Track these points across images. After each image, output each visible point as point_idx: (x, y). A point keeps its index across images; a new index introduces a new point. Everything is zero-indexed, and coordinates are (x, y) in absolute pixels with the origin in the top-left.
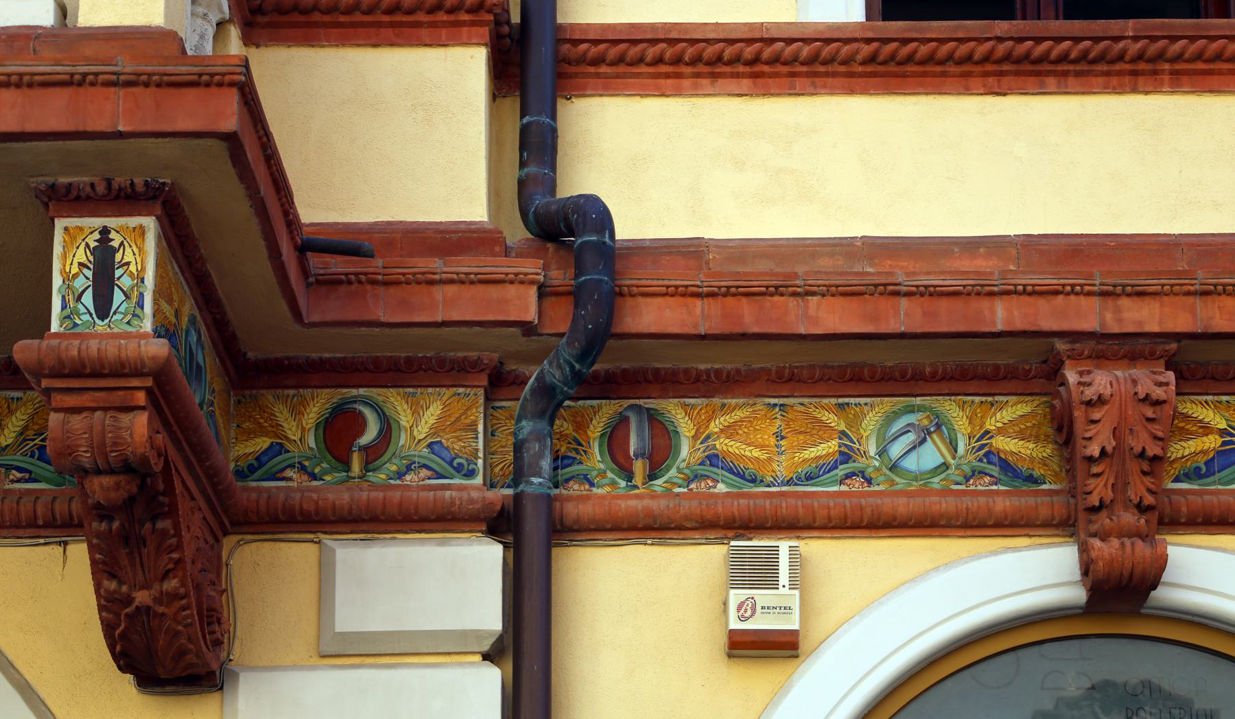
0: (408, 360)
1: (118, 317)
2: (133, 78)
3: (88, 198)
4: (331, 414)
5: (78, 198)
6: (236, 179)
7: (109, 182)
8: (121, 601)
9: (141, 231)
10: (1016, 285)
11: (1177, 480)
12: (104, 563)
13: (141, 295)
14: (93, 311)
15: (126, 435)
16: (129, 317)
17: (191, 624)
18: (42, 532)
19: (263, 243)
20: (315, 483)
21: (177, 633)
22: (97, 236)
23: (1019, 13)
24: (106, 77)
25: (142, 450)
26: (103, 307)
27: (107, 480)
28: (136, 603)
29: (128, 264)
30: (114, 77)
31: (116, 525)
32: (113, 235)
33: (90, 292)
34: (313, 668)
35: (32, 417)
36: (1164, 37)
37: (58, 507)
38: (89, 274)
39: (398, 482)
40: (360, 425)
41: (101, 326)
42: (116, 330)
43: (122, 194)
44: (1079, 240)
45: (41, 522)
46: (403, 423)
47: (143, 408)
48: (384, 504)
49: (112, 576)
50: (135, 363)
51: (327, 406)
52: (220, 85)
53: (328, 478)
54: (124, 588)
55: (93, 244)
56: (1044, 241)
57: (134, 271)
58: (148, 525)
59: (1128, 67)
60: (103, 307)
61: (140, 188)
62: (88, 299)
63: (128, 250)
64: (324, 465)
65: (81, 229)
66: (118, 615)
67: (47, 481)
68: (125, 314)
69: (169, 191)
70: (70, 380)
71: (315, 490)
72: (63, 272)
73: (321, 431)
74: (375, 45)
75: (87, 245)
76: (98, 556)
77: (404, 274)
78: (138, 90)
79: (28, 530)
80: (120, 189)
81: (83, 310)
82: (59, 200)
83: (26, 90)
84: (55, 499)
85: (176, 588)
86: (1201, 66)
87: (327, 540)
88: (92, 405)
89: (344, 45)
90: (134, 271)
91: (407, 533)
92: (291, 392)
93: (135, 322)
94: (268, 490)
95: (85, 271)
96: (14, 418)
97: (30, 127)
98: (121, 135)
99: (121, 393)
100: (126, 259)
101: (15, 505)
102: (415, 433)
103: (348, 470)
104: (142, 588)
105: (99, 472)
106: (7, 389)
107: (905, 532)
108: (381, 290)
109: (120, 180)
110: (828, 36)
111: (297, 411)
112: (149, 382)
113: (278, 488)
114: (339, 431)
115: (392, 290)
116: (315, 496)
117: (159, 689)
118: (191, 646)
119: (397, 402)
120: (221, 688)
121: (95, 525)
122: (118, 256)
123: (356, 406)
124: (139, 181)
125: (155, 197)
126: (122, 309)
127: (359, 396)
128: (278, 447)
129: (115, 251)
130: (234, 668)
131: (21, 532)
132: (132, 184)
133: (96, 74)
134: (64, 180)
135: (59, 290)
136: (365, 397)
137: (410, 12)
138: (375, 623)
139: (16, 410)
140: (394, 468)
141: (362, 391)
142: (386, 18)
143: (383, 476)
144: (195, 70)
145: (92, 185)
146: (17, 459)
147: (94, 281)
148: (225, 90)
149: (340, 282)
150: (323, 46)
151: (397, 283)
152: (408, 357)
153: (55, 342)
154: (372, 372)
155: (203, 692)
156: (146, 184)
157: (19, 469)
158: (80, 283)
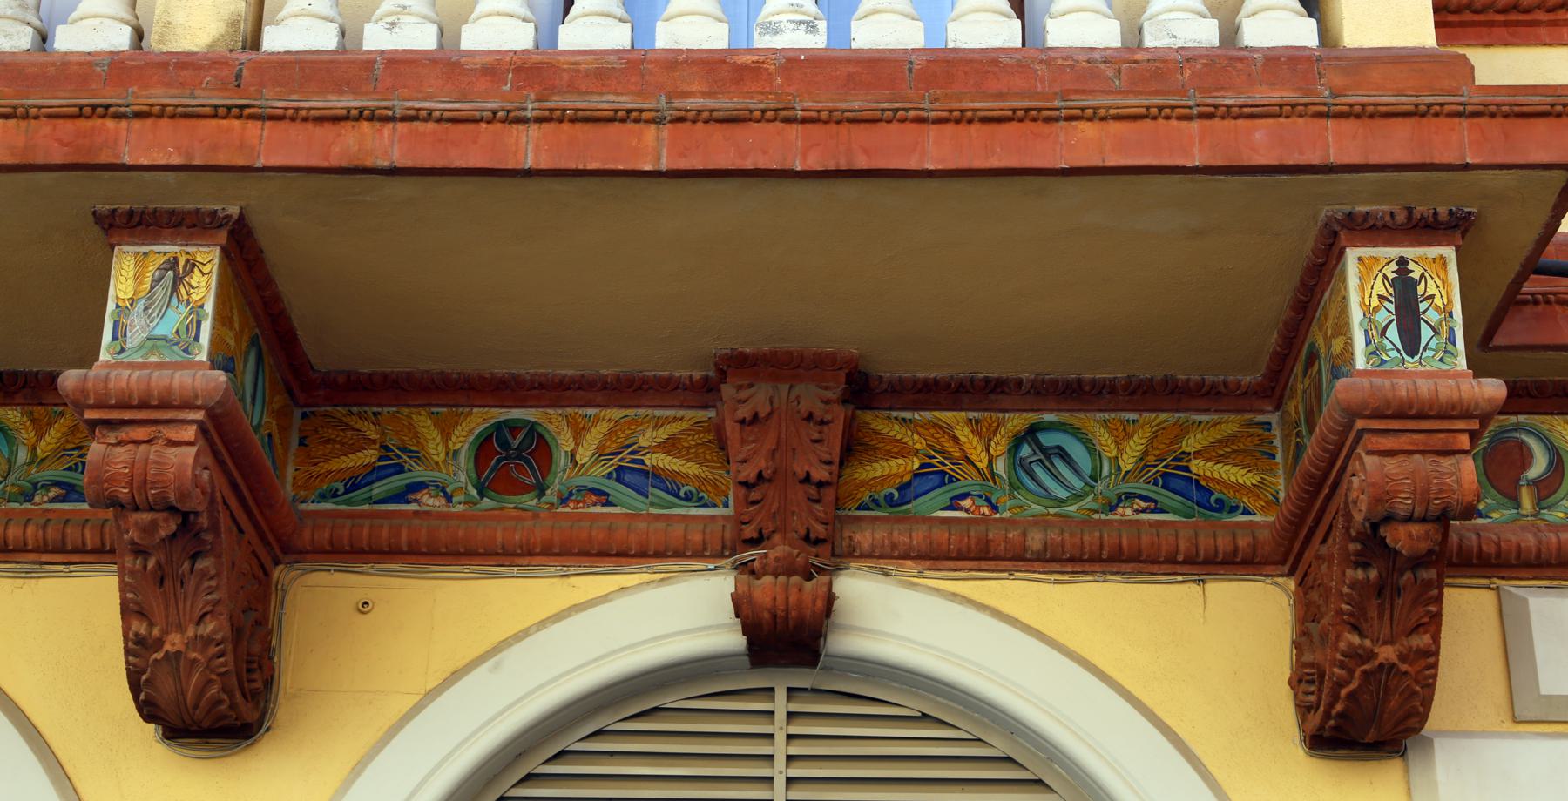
1: (1428, 353)
3: (1385, 226)
6: (1550, 207)
7: (1410, 210)
9: (1443, 261)
12: (1351, 614)
13: (1451, 330)
16: (1441, 354)
18: (1179, 569)
19: (1518, 268)
21: (1415, 693)
24: (1454, 107)
26: (1411, 344)
27: (1416, 529)
28: (1381, 659)
29: (1432, 297)
30: (1461, 108)
31: (1373, 574)
32: (1411, 266)
35: (1151, 441)
38: (1391, 307)
40: (1526, 459)
41: (1411, 363)
42: (1428, 368)
45: (1180, 558)
47: (1465, 452)
49: (1355, 628)
53: (1495, 515)
54: (1368, 643)
55: (1391, 276)
58: (1408, 575)
60: (1411, 344)
62: (1393, 333)
63: (1430, 282)
64: (1489, 501)
65: (1376, 259)
66: (1351, 672)
67: (1175, 512)
72: (1362, 304)
78: (1483, 121)
80: (1422, 218)
81: (1389, 346)
83: (1367, 121)
93: (1448, 359)
97: (1374, 159)
98: (1466, 167)
99: (1442, 436)
103: (1518, 506)
104: (1385, 643)
105: (1409, 519)
109: (1421, 210)
112: (199, 415)
116: (1494, 538)
117: (1330, 753)
121: (1349, 572)
122: (1420, 289)
123: (1524, 437)
124: (1443, 211)
125: (1456, 226)
127: (1518, 424)
129: (1415, 283)
131: (1155, 568)
132: (1435, 214)
133: (1441, 105)
135: (1361, 324)
137: (1527, 11)
139: (1134, 432)
141: (1522, 418)
142: (1501, 18)
144: (1549, 99)
146: (1140, 487)
147: (1419, 319)
155: (1381, 758)
157: (1144, 498)
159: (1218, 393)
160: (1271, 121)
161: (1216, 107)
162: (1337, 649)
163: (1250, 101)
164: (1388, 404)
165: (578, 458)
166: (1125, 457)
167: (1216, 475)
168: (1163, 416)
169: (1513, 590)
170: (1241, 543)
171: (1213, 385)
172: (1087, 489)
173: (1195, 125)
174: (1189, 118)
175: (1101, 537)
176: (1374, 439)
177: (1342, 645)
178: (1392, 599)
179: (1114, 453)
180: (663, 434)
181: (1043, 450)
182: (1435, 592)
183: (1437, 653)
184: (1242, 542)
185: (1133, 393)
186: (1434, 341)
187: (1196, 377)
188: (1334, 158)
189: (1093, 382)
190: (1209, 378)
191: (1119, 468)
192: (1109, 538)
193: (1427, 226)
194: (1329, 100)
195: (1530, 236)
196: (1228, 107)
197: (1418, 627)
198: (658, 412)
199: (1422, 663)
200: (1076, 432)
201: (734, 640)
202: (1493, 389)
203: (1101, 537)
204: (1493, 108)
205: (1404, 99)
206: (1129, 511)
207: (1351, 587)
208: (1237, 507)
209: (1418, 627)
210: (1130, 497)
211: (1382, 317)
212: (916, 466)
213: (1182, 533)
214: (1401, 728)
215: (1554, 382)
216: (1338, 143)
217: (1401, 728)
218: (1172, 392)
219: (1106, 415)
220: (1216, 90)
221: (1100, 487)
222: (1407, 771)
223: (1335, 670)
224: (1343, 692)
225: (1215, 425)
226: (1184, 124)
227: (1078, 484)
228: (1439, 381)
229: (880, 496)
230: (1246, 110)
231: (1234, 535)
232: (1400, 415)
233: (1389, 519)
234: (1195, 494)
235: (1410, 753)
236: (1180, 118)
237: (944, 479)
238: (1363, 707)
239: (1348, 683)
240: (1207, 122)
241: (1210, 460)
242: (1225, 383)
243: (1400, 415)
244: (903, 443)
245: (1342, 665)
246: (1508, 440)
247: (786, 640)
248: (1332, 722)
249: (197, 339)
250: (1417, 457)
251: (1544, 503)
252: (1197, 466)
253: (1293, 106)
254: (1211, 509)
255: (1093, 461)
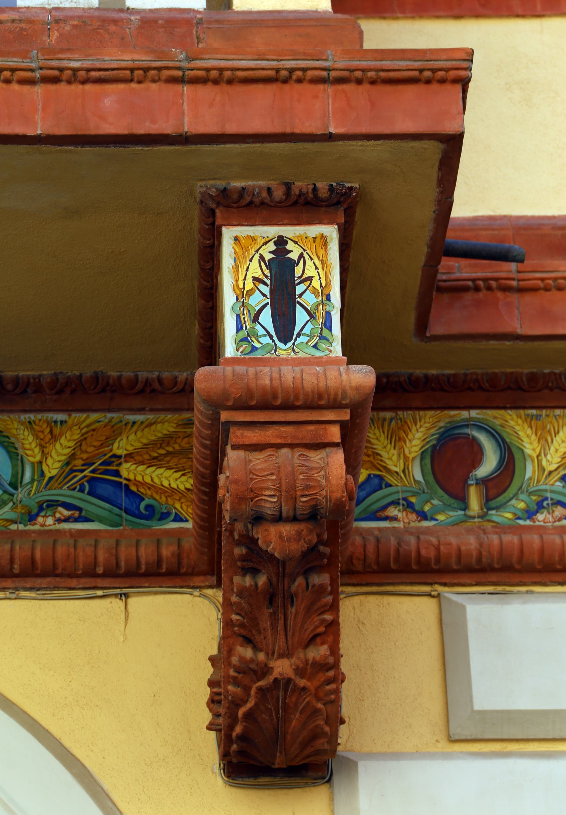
0: (533, 377)
1: (303, 339)
2: (345, 74)
3: (263, 203)
4: (438, 440)
5: (250, 203)
6: (434, 183)
7: (288, 186)
8: (254, 671)
9: (324, 241)
12: (242, 625)
13: (328, 315)
14: (273, 332)
15: (319, 476)
17: (332, 702)
18: (100, 582)
19: (425, 250)
20: (425, 524)
21: (317, 711)
22: (272, 246)
25: (338, 495)
26: (285, 329)
27: (287, 529)
28: (276, 674)
29: (310, 279)
30: (325, 74)
31: (262, 580)
32: (290, 246)
33: (268, 309)
34: (446, 756)
35: (79, 444)
37: (61, 551)
38: (266, 290)
39: (528, 522)
40: (476, 455)
42: (301, 355)
43: (302, 200)
45: (100, 570)
46: (528, 450)
47: (335, 445)
48: (521, 551)
49: (248, 641)
50: (336, 394)
51: (433, 431)
52: (442, 81)
53: (441, 517)
54: (261, 656)
55: (268, 256)
57: (318, 287)
58: (300, 580)
60: (285, 329)
61: (323, 192)
62: (266, 318)
63: (309, 263)
65: (253, 239)
66: (247, 689)
67: (101, 520)
68: (311, 337)
69: (356, 196)
70: (255, 412)
71: (428, 531)
72: (235, 287)
73: (428, 461)
74: (458, 17)
75: (262, 257)
76: (234, 617)
77: (543, 280)
79: (83, 580)
80: (301, 194)
82: (228, 207)
83: (225, 87)
84: (118, 543)
85: (326, 657)
87: (448, 593)
88: (279, 441)
89: (421, 17)
90: (318, 287)
91: (545, 584)
92: (388, 415)
94: (370, 531)
95: (261, 287)
96: (58, 445)
97: (232, 128)
98: (331, 137)
99: (312, 427)
100: (308, 274)
101: (72, 550)
102: (544, 463)
103: (466, 508)
105: (278, 519)
106: (49, 410)
108: (514, 297)
109: (301, 185)
111: (397, 438)
112: (346, 416)
113: (380, 529)
114: (450, 461)
115: (528, 298)
116: (434, 540)
117: (251, 781)
118: (327, 729)
119: (519, 427)
120: (329, 781)
121: (237, 579)
122: (298, 271)
123: (468, 431)
124: (322, 186)
125: (338, 203)
126: (307, 330)
127: (470, 419)
128: (376, 481)
129: (293, 264)
130: (345, 754)
131: (74, 582)
132: (315, 189)
133: (304, 70)
134: (237, 184)
135: (233, 309)
136: (479, 420)
138: (523, 698)
139: (61, 435)
140: (522, 505)
141: (474, 413)
143: (509, 515)
144: (417, 65)
145: (269, 190)
146: (64, 494)
147: (271, 299)
148: (448, 87)
149: (465, 289)
150: (397, 18)
151: (535, 289)
152: (532, 373)
153: (229, 369)
154: (484, 390)
155: (306, 785)
156: (331, 187)
158: (256, 300)
159: (153, 391)
160: (121, 86)
161: (61, 70)
162: (229, 664)
163: (98, 65)
164: (250, 393)
166: (50, 461)
167: (148, 480)
168: (94, 416)
169: (454, 597)
170: (166, 552)
171: (147, 382)
172: (6, 497)
173: (39, 90)
174: (31, 82)
175: (12, 550)
176: (239, 432)
177: (235, 660)
178: (285, 608)
179: (38, 458)
182: (329, 599)
184: (166, 552)
185: (60, 392)
186: (309, 326)
187: (128, 374)
188: (189, 126)
189: (16, 381)
190: (143, 375)
191: (42, 474)
192: (21, 550)
193: (307, 203)
194: (184, 64)
195: (426, 214)
196: (75, 71)
199: (321, 677)
202: (363, 376)
203: (12, 550)
204: (358, 74)
205: (264, 64)
206: (50, 521)
207: (240, 594)
208: (168, 514)
210: (52, 505)
211: (256, 300)
213: (102, 544)
214: (309, 750)
215: (506, 375)
216: (195, 111)
217: (309, 750)
218: (103, 390)
219: (32, 416)
220: (62, 51)
221: (20, 494)
222: (332, 799)
223: (230, 687)
224: (241, 712)
225: (150, 425)
226: (26, 88)
228: (306, 369)
230: (93, 74)
231: (158, 542)
232: (265, 405)
233: (258, 519)
234: (124, 501)
235: (335, 778)
236: (23, 82)
238: (276, 724)
239: (246, 702)
240: (52, 87)
241: (142, 463)
242: (160, 380)
243: (265, 405)
245: (236, 682)
246: (457, 437)
248: (235, 747)
250: (285, 451)
251: (493, 504)
252: (128, 470)
253: (146, 70)
254: (141, 516)
255: (14, 466)
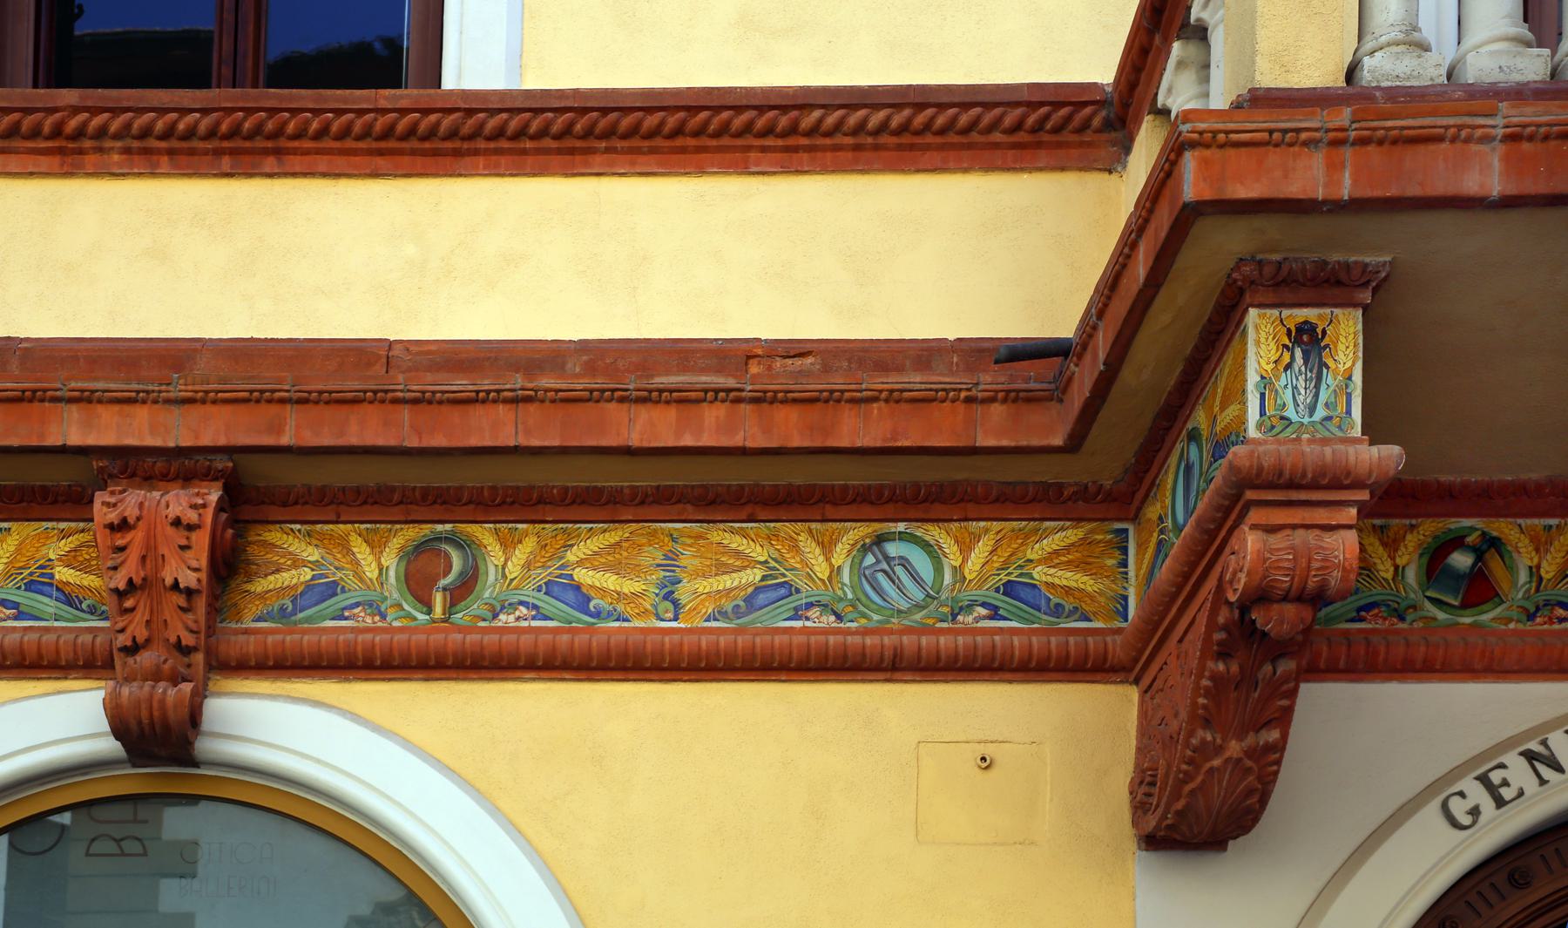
10: (310, 392)
11: (259, 619)
23: (214, 81)
27: (1290, 609)
36: (241, 109)
44: (143, 344)
56: (143, 344)
59: (375, 145)
66: (1198, 768)
67: (300, 622)
86: (457, 144)
107: (951, 675)
110: (967, 100)
112: (1364, 496)
146: (529, 594)
165: (1542, 572)
180: (65, 546)
181: (888, 559)
182: (1292, 685)
183: (1283, 749)
197: (1269, 722)
198: (63, 525)
200: (926, 546)
201: (109, 746)
206: (511, 618)
207: (1212, 678)
209: (1269, 722)
212: (758, 578)
227: (919, 595)
229: (729, 607)
230: (1233, 137)
237: (790, 589)
244: (294, 558)
247: (160, 740)
249: (1349, 412)
